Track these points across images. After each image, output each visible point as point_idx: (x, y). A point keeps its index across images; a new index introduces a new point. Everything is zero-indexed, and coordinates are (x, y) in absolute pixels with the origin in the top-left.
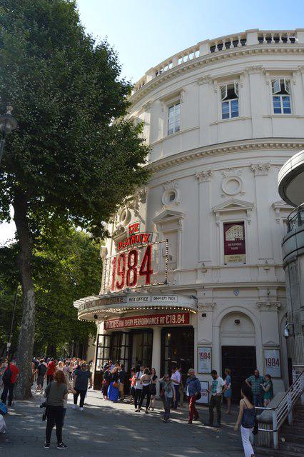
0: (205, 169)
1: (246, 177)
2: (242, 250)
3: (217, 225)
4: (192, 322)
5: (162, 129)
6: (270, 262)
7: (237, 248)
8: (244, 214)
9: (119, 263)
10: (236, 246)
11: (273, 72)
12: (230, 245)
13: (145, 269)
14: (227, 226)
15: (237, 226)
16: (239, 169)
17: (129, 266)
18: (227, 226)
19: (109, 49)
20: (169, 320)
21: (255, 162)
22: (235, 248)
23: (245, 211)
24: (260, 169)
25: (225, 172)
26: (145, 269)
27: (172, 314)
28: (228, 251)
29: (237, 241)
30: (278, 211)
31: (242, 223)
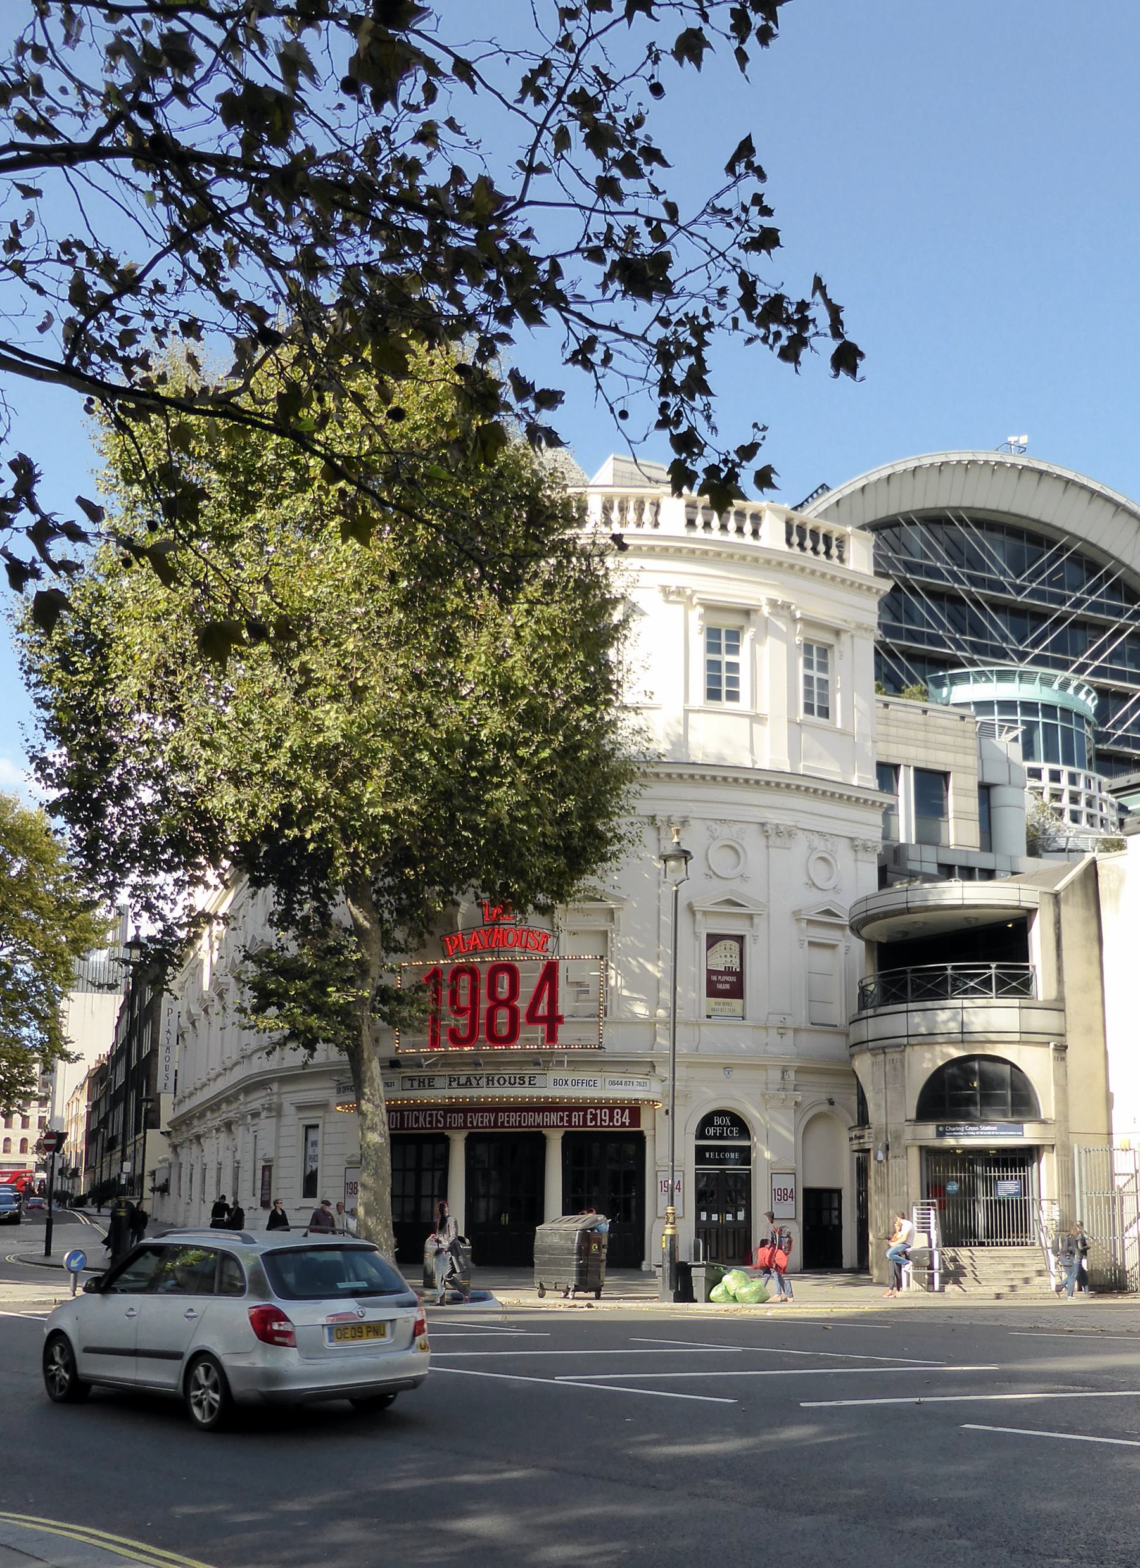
0: (677, 811)
1: (752, 843)
2: (737, 991)
3: (696, 935)
4: (645, 1126)
5: (950, 1142)
6: (790, 1023)
7: (727, 986)
8: (747, 922)
9: (600, 1554)
10: (726, 982)
11: (808, 623)
12: (714, 978)
13: (542, 1010)
14: (713, 940)
15: (728, 943)
16: (739, 826)
17: (492, 994)
18: (713, 940)
19: (36, 471)
20: (594, 1118)
21: (773, 818)
22: (727, 986)
23: (751, 917)
24: (778, 834)
25: (714, 826)
26: (542, 1010)
27: (601, 1108)
28: (713, 991)
29: (728, 972)
30: (804, 924)
31: (740, 939)
